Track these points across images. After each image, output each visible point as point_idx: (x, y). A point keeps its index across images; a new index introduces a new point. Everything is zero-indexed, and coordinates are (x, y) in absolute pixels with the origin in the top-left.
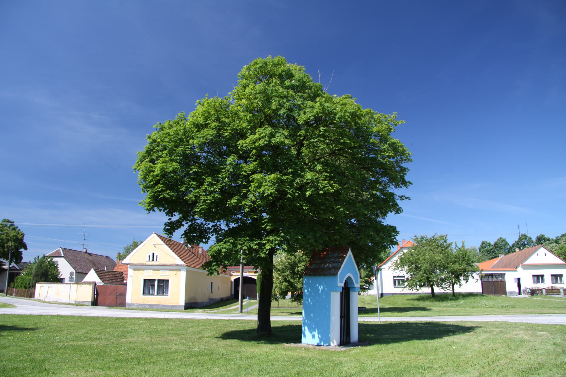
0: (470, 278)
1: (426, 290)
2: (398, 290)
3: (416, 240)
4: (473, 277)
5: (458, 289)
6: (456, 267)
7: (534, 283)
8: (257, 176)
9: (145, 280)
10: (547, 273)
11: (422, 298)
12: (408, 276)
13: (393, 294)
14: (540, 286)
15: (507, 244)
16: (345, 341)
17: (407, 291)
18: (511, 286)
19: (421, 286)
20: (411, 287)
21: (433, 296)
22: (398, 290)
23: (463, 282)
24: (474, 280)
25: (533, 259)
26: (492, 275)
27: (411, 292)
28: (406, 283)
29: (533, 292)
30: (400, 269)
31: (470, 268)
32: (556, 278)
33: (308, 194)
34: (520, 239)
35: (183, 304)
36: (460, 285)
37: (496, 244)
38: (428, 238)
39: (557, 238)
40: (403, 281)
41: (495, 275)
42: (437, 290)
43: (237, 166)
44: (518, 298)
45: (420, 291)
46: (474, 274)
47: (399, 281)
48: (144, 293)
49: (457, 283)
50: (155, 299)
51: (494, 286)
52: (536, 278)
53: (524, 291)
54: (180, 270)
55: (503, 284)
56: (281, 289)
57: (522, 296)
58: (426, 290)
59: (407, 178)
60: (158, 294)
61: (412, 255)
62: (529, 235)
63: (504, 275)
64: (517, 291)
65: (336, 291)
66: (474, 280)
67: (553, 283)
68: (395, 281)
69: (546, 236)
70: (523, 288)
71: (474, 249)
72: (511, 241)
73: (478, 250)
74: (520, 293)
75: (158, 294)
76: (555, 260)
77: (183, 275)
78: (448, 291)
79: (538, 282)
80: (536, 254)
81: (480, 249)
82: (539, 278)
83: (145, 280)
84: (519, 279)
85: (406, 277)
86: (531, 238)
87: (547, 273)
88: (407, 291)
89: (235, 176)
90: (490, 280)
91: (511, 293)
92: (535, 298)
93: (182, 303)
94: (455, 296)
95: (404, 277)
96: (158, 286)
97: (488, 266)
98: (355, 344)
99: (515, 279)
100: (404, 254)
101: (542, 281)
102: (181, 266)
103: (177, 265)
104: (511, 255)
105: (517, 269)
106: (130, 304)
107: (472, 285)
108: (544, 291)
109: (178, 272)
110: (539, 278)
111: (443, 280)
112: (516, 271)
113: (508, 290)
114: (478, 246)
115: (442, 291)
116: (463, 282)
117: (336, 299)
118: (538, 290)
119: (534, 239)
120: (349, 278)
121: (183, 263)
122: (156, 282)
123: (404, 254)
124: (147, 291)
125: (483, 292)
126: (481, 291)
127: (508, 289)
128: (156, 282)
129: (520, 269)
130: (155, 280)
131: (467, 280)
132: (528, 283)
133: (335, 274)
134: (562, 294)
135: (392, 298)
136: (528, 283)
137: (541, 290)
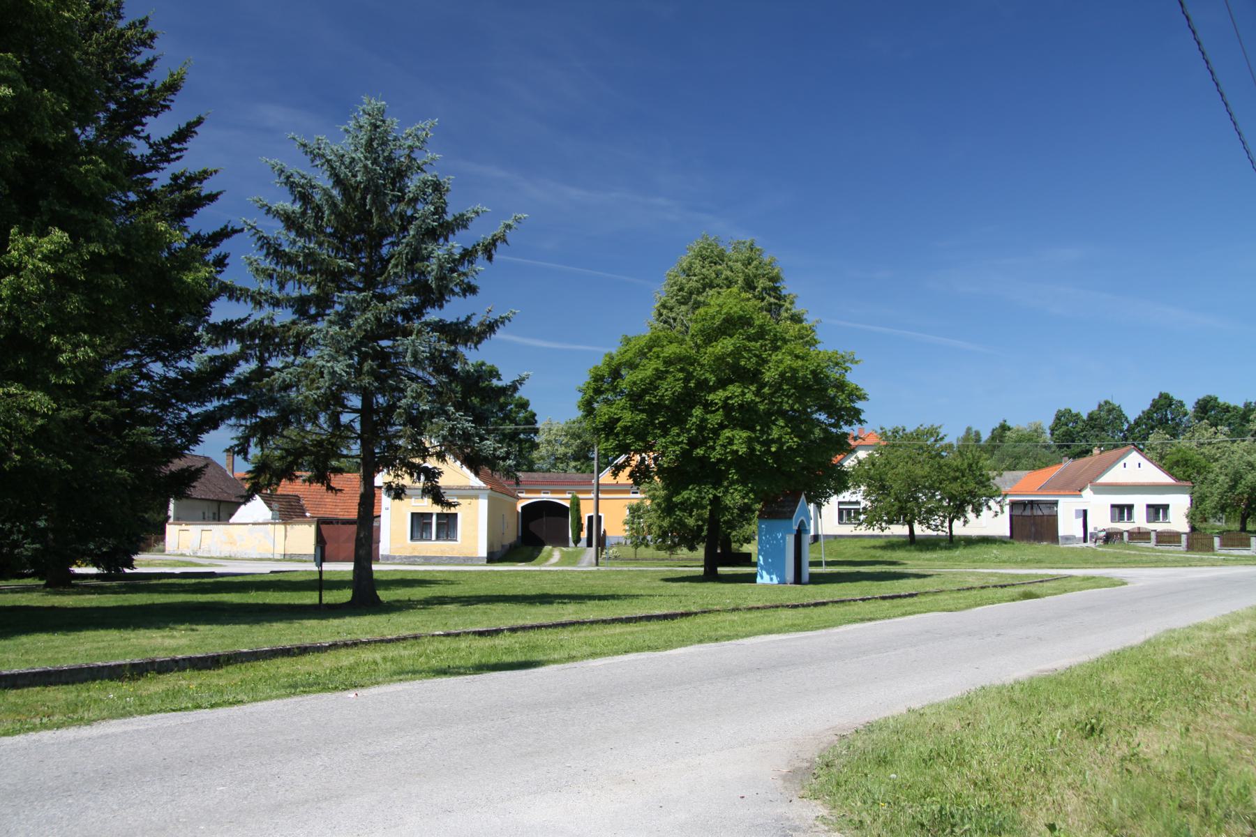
0: (985, 509)
1: (900, 530)
2: (847, 530)
3: (884, 434)
4: (989, 508)
5: (959, 528)
6: (955, 488)
7: (1113, 520)
8: (727, 433)
9: (413, 514)
10: (1140, 502)
11: (893, 544)
12: (865, 503)
13: (836, 537)
14: (1124, 526)
15: (1120, 416)
16: (798, 580)
17: (862, 530)
18: (1068, 525)
19: (890, 522)
20: (870, 524)
21: (912, 541)
22: (847, 530)
23: (971, 515)
24: (991, 513)
25: (1115, 475)
26: (1032, 502)
27: (870, 532)
28: (862, 517)
29: (1110, 537)
30: (852, 490)
31: (983, 491)
32: (1157, 511)
33: (773, 449)
34: (1153, 406)
35: (485, 555)
36: (966, 522)
37: (1091, 417)
38: (908, 431)
39: (1247, 405)
40: (857, 512)
41: (1038, 503)
42: (919, 530)
43: (703, 420)
44: (1083, 549)
45: (887, 532)
46: (992, 503)
47: (849, 511)
48: (412, 538)
49: (959, 519)
50: (433, 547)
51: (1034, 524)
52: (1117, 511)
53: (1092, 537)
54: (477, 497)
55: (1052, 521)
56: (660, 527)
57: (1089, 544)
58: (900, 530)
59: (862, 417)
60: (438, 538)
61: (873, 465)
62: (1176, 396)
63: (1056, 503)
64: (1081, 535)
65: (790, 533)
66: (991, 513)
67: (1148, 521)
68: (840, 512)
69: (1221, 401)
70: (1090, 530)
71: (1037, 431)
72: (1133, 410)
73: (1048, 431)
74: (1085, 540)
75: (438, 538)
76: (1158, 476)
77: (483, 504)
78: (940, 533)
79: (1121, 519)
80: (1121, 463)
81: (1053, 430)
82: (1122, 511)
83: (413, 514)
84: (1085, 512)
85: (862, 505)
86: (1182, 404)
87: (1140, 502)
88: (862, 530)
89: (701, 427)
90: (1028, 512)
91: (1068, 539)
92: (1109, 549)
93: (483, 552)
94: (952, 542)
95: (857, 503)
96: (438, 524)
97: (1022, 484)
98: (805, 584)
99: (1077, 511)
100: (859, 462)
101: (1130, 517)
102: (479, 489)
103: (472, 488)
104: (1087, 459)
105: (1083, 493)
106: (387, 558)
107: (992, 521)
108: (1126, 535)
109: (474, 501)
110: (1122, 511)
111: (931, 512)
112: (1080, 496)
113: (1060, 534)
114: (1047, 422)
115: (935, 533)
116: (971, 515)
117: (790, 540)
118: (1116, 533)
119: (1190, 407)
120: (802, 522)
121: (482, 484)
122: (434, 518)
123: (859, 462)
124: (417, 534)
125: (1011, 536)
126: (1008, 534)
127: (1062, 531)
128: (434, 518)
129: (1087, 493)
130: (431, 514)
131: (977, 511)
132: (1101, 521)
133: (791, 518)
134: (1152, 543)
135: (834, 545)
136: (1101, 521)
137: (1122, 534)
